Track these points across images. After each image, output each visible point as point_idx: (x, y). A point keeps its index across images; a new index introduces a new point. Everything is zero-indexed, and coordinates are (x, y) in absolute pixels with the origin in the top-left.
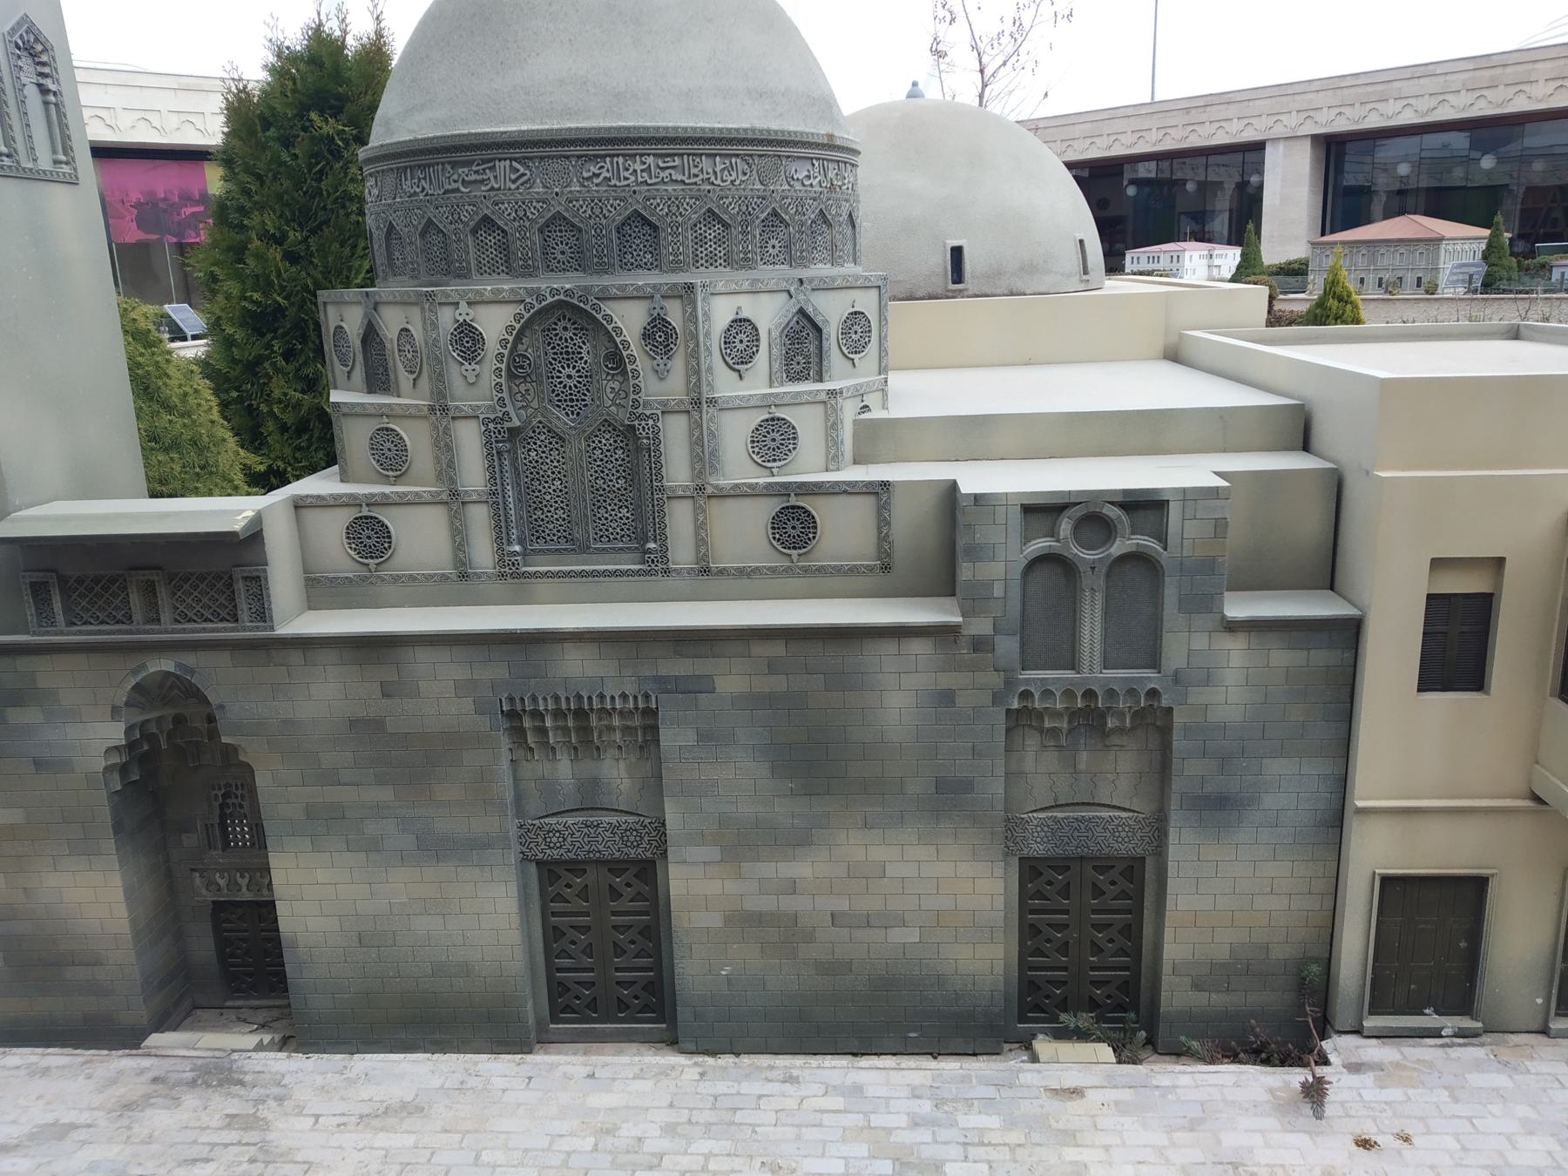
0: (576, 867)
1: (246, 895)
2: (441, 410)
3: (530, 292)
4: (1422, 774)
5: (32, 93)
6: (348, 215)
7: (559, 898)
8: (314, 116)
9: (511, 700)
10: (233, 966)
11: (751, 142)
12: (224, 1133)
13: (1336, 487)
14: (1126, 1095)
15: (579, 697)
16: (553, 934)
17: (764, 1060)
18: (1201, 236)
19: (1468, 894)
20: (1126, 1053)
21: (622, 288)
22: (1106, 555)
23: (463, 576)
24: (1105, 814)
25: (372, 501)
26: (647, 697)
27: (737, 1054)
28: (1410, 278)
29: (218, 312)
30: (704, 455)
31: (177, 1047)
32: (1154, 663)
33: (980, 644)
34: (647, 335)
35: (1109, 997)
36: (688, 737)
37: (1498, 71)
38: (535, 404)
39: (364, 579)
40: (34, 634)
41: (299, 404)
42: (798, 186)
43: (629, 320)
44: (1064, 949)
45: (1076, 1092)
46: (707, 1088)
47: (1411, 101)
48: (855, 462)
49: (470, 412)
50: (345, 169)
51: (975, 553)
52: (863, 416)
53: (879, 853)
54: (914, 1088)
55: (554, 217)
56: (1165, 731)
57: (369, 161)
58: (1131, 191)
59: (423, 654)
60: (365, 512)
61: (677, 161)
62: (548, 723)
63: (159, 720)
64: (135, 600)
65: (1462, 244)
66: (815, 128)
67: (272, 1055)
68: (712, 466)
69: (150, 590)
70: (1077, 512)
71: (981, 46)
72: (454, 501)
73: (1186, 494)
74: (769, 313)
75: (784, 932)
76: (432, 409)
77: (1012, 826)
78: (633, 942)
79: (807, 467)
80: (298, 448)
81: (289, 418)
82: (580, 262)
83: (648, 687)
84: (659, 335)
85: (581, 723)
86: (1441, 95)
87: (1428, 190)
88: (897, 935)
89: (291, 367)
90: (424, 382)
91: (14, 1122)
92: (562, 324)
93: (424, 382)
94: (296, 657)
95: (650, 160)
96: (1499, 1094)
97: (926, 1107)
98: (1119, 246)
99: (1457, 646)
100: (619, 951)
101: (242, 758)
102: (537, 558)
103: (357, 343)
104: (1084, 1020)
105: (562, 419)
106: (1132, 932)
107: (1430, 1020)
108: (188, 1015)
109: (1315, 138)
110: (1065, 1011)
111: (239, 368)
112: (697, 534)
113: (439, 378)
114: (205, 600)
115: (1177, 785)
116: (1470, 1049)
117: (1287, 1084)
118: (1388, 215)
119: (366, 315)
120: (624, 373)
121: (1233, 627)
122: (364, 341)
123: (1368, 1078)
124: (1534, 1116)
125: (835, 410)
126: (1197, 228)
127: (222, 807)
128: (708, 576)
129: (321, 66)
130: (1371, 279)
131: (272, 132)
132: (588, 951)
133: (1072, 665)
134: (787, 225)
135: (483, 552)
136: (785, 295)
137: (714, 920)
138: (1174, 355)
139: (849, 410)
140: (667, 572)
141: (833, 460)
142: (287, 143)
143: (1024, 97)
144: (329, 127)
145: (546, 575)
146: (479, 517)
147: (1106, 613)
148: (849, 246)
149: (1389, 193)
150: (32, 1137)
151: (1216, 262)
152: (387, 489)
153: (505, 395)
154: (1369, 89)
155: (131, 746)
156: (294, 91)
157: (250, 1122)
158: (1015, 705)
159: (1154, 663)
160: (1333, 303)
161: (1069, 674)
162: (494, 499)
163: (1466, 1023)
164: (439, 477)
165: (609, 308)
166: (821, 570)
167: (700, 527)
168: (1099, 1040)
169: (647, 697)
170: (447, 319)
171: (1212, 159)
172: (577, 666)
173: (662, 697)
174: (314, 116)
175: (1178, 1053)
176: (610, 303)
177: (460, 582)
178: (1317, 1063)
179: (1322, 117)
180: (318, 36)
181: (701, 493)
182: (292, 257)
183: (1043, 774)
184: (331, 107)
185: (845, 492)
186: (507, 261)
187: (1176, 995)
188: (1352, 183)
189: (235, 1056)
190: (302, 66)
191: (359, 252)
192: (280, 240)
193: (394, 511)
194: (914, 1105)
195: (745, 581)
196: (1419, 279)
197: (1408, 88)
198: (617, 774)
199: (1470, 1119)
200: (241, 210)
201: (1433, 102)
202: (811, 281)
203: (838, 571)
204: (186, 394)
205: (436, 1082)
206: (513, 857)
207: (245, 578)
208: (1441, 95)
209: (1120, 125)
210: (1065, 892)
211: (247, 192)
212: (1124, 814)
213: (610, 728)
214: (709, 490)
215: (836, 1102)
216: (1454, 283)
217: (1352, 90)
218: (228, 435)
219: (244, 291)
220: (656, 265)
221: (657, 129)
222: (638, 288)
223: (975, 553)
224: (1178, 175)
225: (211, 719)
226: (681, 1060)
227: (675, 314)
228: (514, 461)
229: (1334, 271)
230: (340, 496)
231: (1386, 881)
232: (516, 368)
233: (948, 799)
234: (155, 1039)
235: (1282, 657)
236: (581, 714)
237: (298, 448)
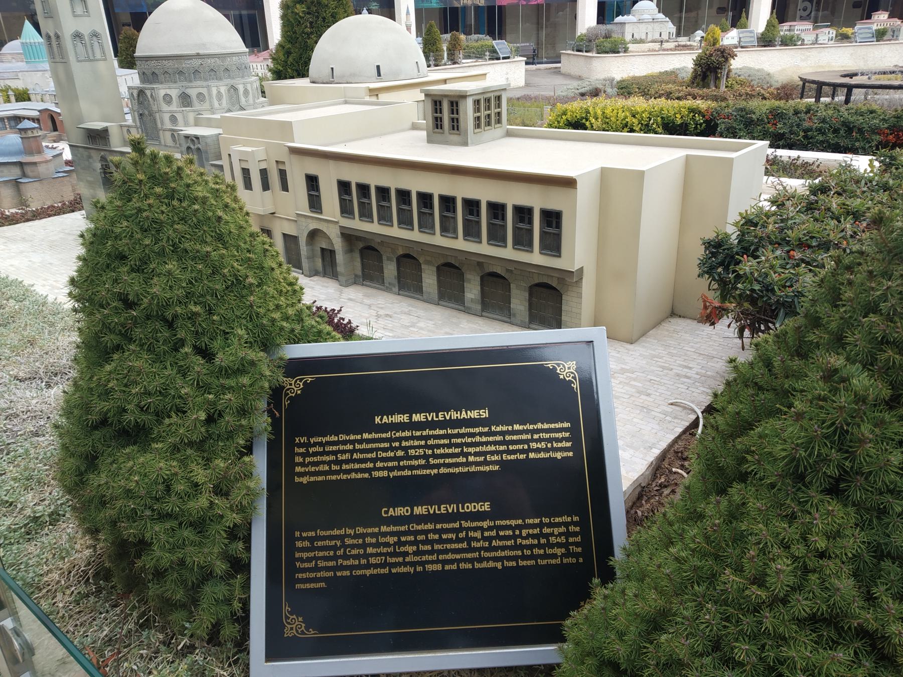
5: (96, 45)
74: (174, 93)
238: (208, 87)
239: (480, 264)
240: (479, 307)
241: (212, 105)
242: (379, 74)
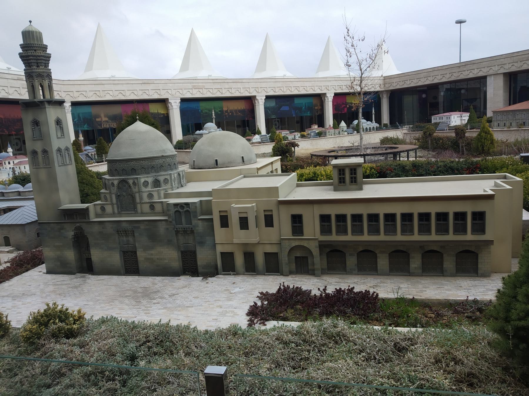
0: (127, 252)
5: (67, 155)
16: (125, 261)
30: (141, 198)
33: (171, 222)
43: (131, 182)
72: (112, 204)
74: (150, 180)
84: (134, 183)
85: (126, 233)
88: (165, 261)
105: (124, 194)
109: (505, 74)
128: (143, 214)
135: (116, 211)
137: (143, 259)
141: (159, 198)
146: (115, 206)
154: (523, 56)
155: (75, 235)
160: (483, 134)
162: (117, 204)
167: (141, 207)
170: (110, 182)
172: (124, 225)
177: (113, 215)
179: (506, 67)
181: (141, 203)
187: (200, 270)
198: (131, 239)
203: (158, 213)
209: (436, 73)
217: (517, 57)
231: (221, 253)
232: (119, 187)
233: (169, 243)
235: (206, 223)
236: (125, 231)
238: (170, 175)
239: (421, 247)
240: (420, 271)
241: (172, 185)
242: (243, 162)
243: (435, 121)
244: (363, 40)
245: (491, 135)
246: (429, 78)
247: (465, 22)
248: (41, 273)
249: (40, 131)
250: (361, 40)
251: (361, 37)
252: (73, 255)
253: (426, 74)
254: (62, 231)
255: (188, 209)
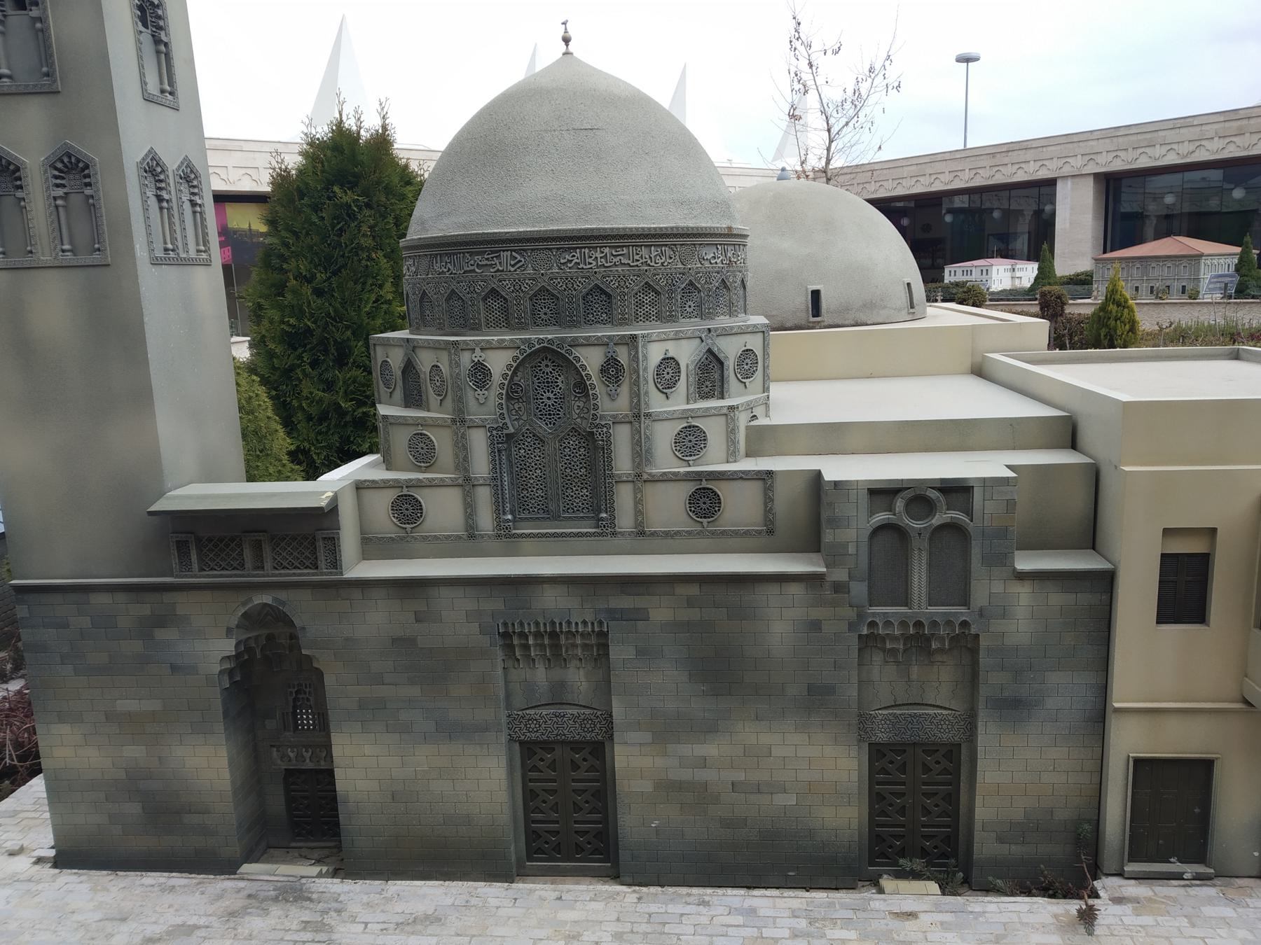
0: (547, 746)
1: (309, 765)
2: (460, 422)
3: (524, 341)
4: (1159, 680)
5: (187, 206)
6: (360, 261)
7: (535, 768)
8: (336, 189)
9: (505, 624)
10: (301, 819)
11: (675, 236)
12: (302, 934)
13: (1095, 476)
14: (948, 917)
15: (553, 623)
16: (530, 795)
17: (684, 890)
18: (1006, 254)
19: (1198, 774)
20: (947, 888)
21: (586, 338)
22: (928, 527)
23: (472, 536)
24: (931, 711)
25: (410, 484)
26: (601, 623)
27: (662, 886)
28: (1176, 286)
29: (264, 332)
30: (641, 452)
31: (263, 874)
32: (965, 602)
33: (839, 588)
34: (603, 371)
35: (936, 847)
36: (630, 653)
37: (1245, 122)
38: (524, 417)
39: (402, 539)
40: (177, 577)
41: (321, 400)
42: (707, 264)
43: (591, 360)
44: (902, 811)
45: (912, 915)
46: (643, 908)
47: (1174, 146)
48: (747, 455)
49: (480, 423)
50: (359, 227)
51: (835, 523)
52: (753, 423)
53: (766, 739)
54: (793, 911)
55: (540, 290)
56: (974, 652)
57: (408, 248)
58: (948, 218)
59: (445, 592)
60: (405, 492)
61: (625, 251)
62: (531, 642)
63: (257, 638)
64: (248, 554)
65: (1218, 259)
66: (720, 224)
67: (330, 880)
68: (648, 460)
69: (258, 547)
70: (908, 494)
71: (829, 111)
72: (467, 484)
73: (986, 482)
74: (687, 354)
75: (693, 795)
76: (454, 421)
77: (863, 721)
78: (587, 802)
79: (714, 461)
80: (320, 433)
81: (314, 411)
82: (558, 319)
83: (602, 617)
84: (612, 370)
85: (554, 643)
86: (1198, 141)
87: (1190, 214)
89: (315, 373)
90: (449, 402)
91: (155, 923)
92: (544, 363)
93: (449, 402)
94: (356, 593)
95: (607, 250)
96: (1226, 922)
97: (803, 924)
98: (940, 261)
99: (1184, 589)
100: (577, 808)
101: (315, 665)
102: (522, 524)
103: (400, 373)
104: (918, 864)
105: (543, 428)
106: (952, 798)
107: (1175, 867)
108: (264, 852)
109: (1097, 177)
110: (904, 857)
111: (278, 373)
112: (636, 507)
113: (459, 400)
114: (295, 554)
115: (984, 691)
116: (1205, 889)
117: (1067, 912)
118: (1158, 237)
119: (406, 354)
120: (587, 395)
121: (1022, 576)
122: (403, 372)
123: (1127, 909)
124: (1251, 937)
125: (733, 420)
126: (1002, 246)
127: (295, 700)
128: (645, 537)
129: (342, 152)
130: (1144, 288)
131: (306, 200)
132: (555, 808)
133: (906, 602)
134: (699, 291)
135: (486, 520)
136: (698, 341)
137: (646, 786)
138: (980, 371)
139: (743, 419)
140: (614, 534)
141: (731, 456)
142: (316, 208)
143: (859, 149)
144: (348, 197)
145: (529, 536)
146: (484, 496)
147: (930, 565)
148: (741, 303)
149: (1158, 217)
150: (169, 933)
151: (1018, 274)
152: (421, 476)
153: (505, 411)
154: (1140, 137)
155: (238, 656)
156: (322, 172)
157: (320, 927)
158: (865, 632)
159: (965, 602)
161: (903, 610)
163: (1201, 869)
164: (457, 468)
165: (577, 352)
166: (723, 533)
167: (638, 502)
168: (929, 879)
169: (601, 623)
170: (466, 359)
171: (1014, 193)
172: (551, 600)
173: (612, 623)
174: (336, 189)
175: (988, 889)
176: (579, 349)
178: (1089, 897)
179: (1102, 159)
180: (340, 131)
181: (640, 479)
182: (318, 292)
183: (885, 679)
184: (349, 182)
185: (741, 478)
186: (508, 321)
187: (985, 846)
188: (1128, 210)
189: (304, 881)
190: (329, 153)
191: (368, 287)
192: (309, 280)
193: (427, 491)
194: (794, 923)
195: (670, 541)
196: (1184, 287)
197: (1171, 136)
198: (578, 679)
199: (1203, 939)
200: (282, 258)
201: (1192, 147)
202: (716, 330)
203: (736, 534)
204: (250, 398)
205: (449, 901)
206: (504, 738)
207: (324, 539)
208: (1198, 141)
209: (939, 167)
210: (903, 768)
211: (286, 245)
212: (945, 712)
213: (574, 646)
214: (645, 477)
215: (739, 920)
216: (1211, 291)
217: (1126, 139)
218: (279, 427)
219: (283, 316)
220: (610, 321)
221: (612, 229)
222: (598, 338)
223: (835, 523)
224: (987, 205)
225: (293, 637)
226: (624, 888)
227: (623, 355)
228: (509, 456)
229: (1114, 283)
230: (388, 481)
231: (1138, 762)
232: (513, 392)
233: (816, 700)
234: (246, 868)
235: (1057, 598)
236: (554, 635)
237: (320, 433)
243: (953, 279)
244: (836, 52)
245: (1131, 310)
246: (921, 179)
247: (976, 59)
248: (22, 864)
249: (41, 34)
250: (829, 52)
251: (831, 44)
252: (224, 762)
253: (914, 168)
254: (161, 634)
255: (960, 516)
